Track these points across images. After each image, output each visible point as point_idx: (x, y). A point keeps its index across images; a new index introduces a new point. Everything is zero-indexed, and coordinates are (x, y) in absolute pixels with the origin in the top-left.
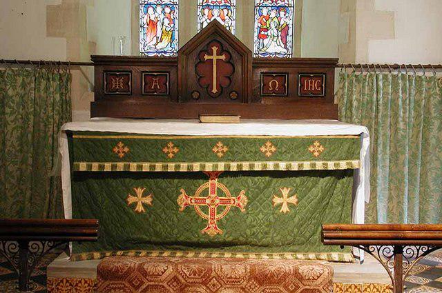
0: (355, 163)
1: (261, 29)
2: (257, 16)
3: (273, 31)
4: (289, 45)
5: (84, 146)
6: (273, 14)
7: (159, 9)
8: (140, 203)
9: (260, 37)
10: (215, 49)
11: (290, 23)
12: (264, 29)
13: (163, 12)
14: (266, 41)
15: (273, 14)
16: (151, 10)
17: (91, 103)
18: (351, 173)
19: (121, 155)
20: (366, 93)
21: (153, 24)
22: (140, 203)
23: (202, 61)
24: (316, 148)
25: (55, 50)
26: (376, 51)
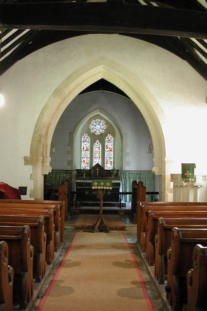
3: (109, 162)
5: (78, 184)
21: (84, 161)
25: (69, 168)
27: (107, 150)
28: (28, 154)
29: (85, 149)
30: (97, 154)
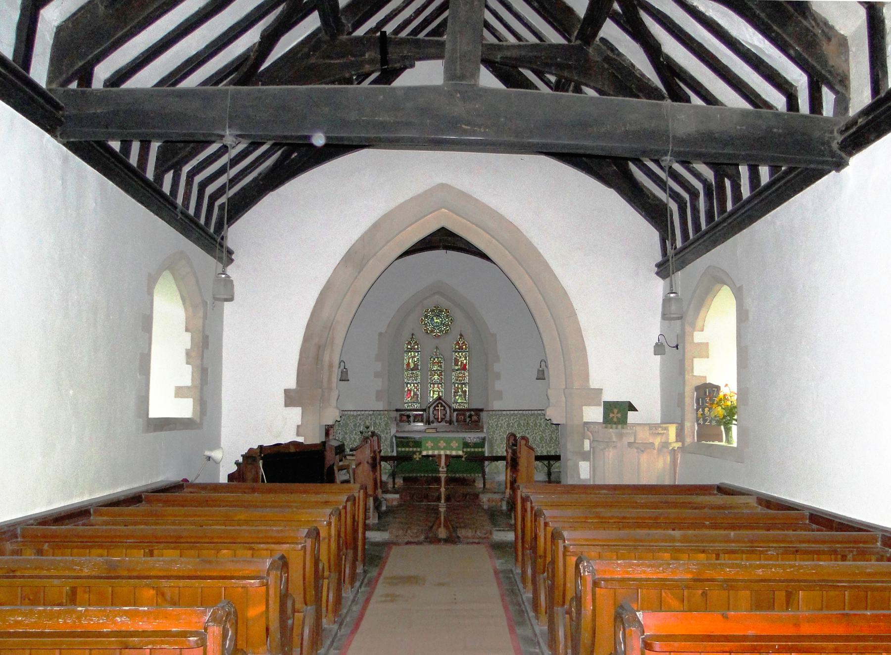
0: (483, 450)
1: (455, 392)
2: (453, 387)
3: (460, 393)
4: (467, 399)
6: (460, 386)
7: (412, 385)
8: (613, 415)
9: (455, 396)
10: (439, 405)
11: (467, 390)
12: (456, 392)
13: (414, 386)
14: (457, 397)
15: (460, 386)
16: (409, 385)
17: (287, 391)
18: (844, 609)
19: (442, 447)
20: (443, 476)
21: (410, 391)
22: (613, 415)
23: (435, 410)
24: (59, 587)
26: (497, 405)
27: (457, 368)
28: (292, 384)
29: (412, 366)
30: (436, 377)
